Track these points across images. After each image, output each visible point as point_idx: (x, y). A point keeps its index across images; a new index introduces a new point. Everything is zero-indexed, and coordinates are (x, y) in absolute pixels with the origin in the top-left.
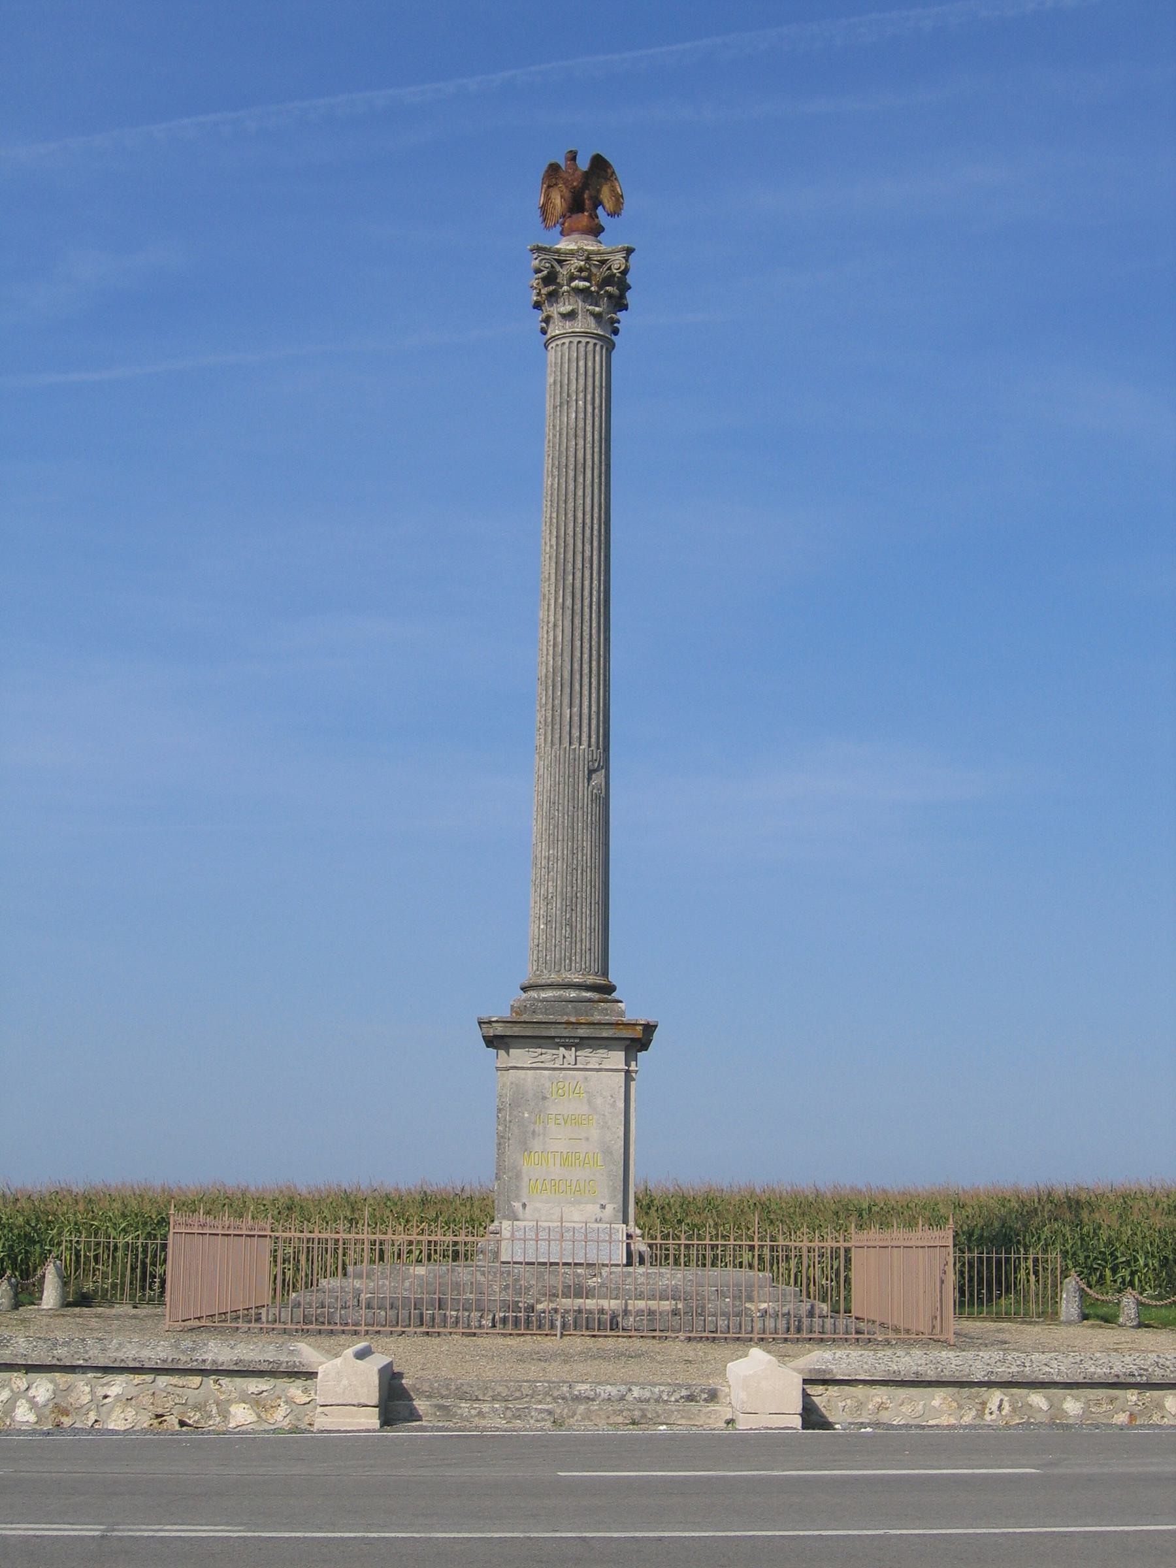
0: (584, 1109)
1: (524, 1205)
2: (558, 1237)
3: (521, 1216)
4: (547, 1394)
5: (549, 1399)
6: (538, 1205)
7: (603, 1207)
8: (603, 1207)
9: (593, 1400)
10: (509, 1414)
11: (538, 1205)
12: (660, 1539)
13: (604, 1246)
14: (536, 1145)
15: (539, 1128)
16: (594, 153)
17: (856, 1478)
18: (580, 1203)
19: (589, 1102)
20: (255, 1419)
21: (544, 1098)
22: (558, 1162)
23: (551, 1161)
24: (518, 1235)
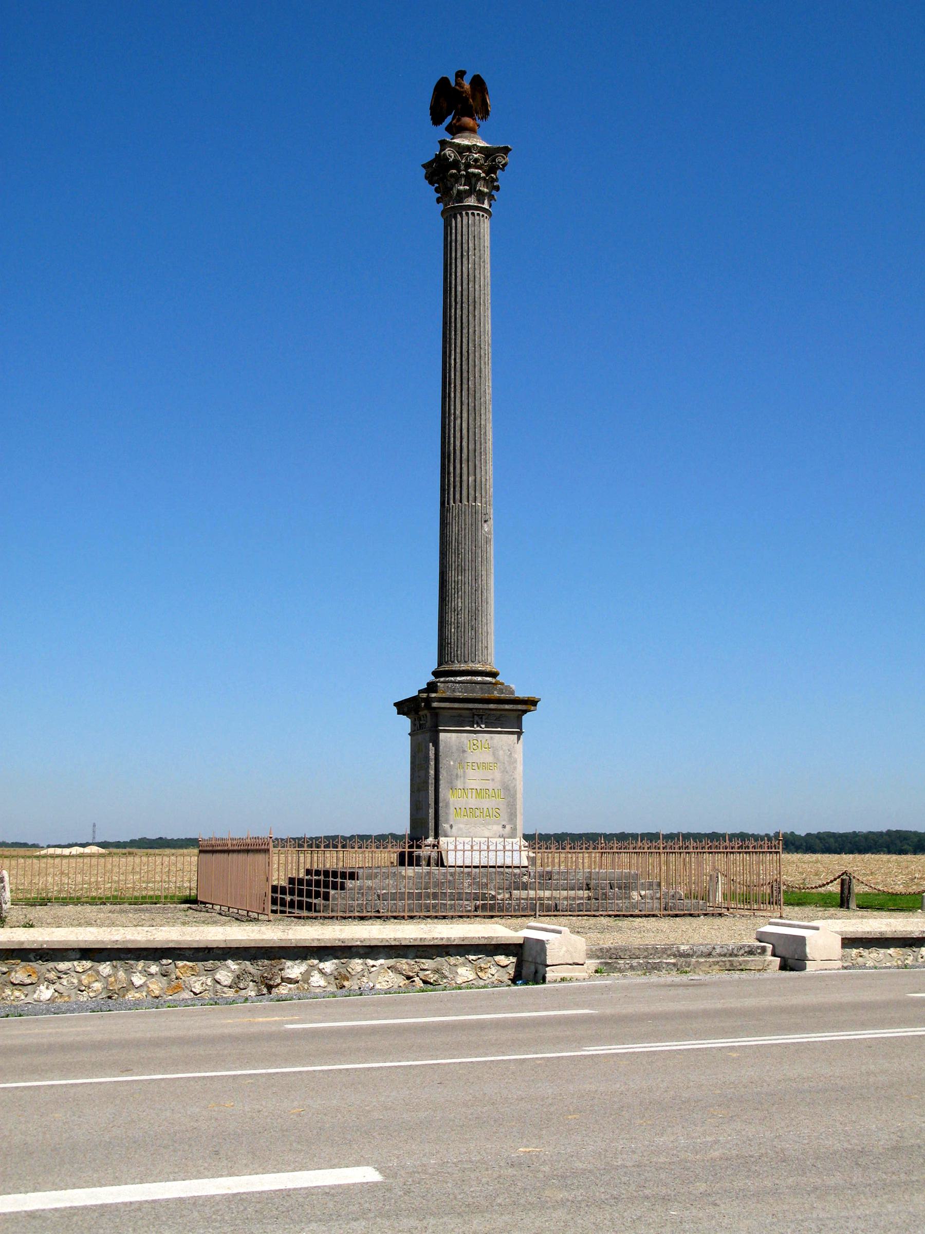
0: (490, 759)
1: (451, 826)
2: (502, 848)
3: (449, 834)
4: (664, 953)
5: (665, 956)
6: (462, 826)
7: (504, 827)
8: (504, 827)
9: (692, 956)
10: (649, 966)
11: (462, 826)
12: (235, 1077)
13: (500, 854)
14: (459, 784)
15: (460, 772)
16: (434, 127)
17: (361, 1028)
18: (489, 824)
19: (494, 754)
20: (475, 977)
21: (464, 751)
22: (474, 796)
23: (470, 795)
24: (460, 847)
